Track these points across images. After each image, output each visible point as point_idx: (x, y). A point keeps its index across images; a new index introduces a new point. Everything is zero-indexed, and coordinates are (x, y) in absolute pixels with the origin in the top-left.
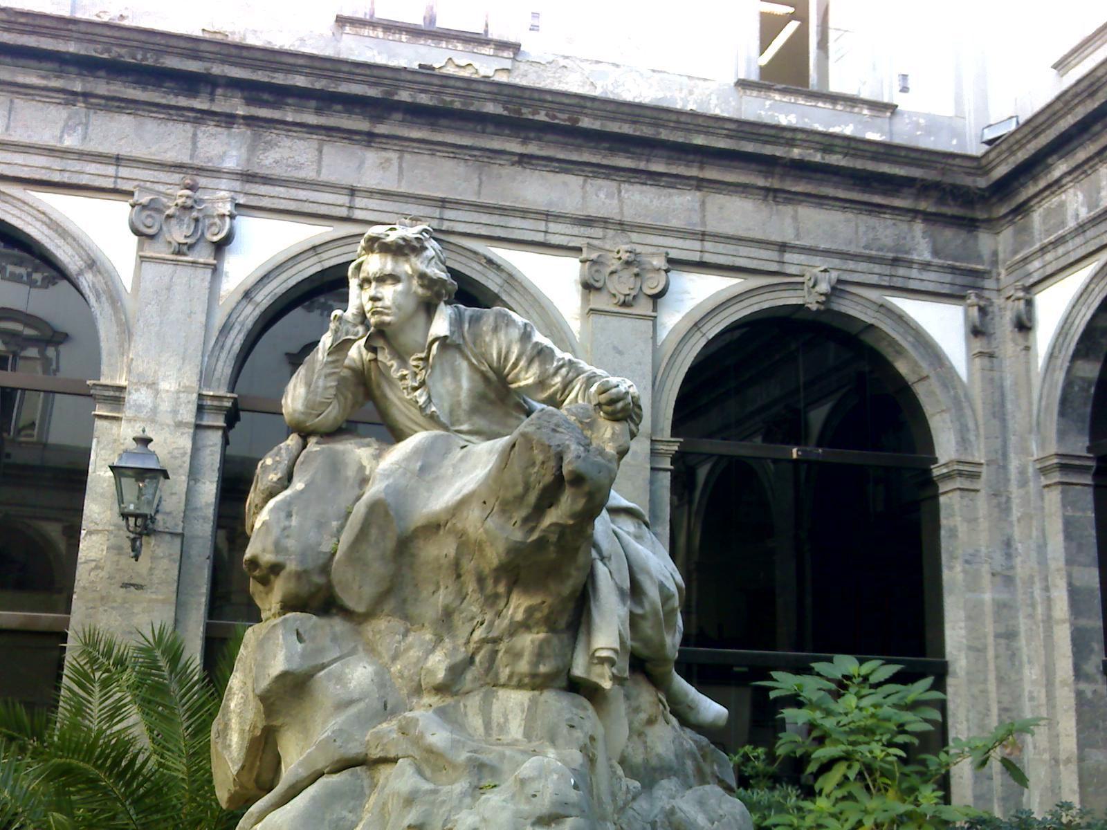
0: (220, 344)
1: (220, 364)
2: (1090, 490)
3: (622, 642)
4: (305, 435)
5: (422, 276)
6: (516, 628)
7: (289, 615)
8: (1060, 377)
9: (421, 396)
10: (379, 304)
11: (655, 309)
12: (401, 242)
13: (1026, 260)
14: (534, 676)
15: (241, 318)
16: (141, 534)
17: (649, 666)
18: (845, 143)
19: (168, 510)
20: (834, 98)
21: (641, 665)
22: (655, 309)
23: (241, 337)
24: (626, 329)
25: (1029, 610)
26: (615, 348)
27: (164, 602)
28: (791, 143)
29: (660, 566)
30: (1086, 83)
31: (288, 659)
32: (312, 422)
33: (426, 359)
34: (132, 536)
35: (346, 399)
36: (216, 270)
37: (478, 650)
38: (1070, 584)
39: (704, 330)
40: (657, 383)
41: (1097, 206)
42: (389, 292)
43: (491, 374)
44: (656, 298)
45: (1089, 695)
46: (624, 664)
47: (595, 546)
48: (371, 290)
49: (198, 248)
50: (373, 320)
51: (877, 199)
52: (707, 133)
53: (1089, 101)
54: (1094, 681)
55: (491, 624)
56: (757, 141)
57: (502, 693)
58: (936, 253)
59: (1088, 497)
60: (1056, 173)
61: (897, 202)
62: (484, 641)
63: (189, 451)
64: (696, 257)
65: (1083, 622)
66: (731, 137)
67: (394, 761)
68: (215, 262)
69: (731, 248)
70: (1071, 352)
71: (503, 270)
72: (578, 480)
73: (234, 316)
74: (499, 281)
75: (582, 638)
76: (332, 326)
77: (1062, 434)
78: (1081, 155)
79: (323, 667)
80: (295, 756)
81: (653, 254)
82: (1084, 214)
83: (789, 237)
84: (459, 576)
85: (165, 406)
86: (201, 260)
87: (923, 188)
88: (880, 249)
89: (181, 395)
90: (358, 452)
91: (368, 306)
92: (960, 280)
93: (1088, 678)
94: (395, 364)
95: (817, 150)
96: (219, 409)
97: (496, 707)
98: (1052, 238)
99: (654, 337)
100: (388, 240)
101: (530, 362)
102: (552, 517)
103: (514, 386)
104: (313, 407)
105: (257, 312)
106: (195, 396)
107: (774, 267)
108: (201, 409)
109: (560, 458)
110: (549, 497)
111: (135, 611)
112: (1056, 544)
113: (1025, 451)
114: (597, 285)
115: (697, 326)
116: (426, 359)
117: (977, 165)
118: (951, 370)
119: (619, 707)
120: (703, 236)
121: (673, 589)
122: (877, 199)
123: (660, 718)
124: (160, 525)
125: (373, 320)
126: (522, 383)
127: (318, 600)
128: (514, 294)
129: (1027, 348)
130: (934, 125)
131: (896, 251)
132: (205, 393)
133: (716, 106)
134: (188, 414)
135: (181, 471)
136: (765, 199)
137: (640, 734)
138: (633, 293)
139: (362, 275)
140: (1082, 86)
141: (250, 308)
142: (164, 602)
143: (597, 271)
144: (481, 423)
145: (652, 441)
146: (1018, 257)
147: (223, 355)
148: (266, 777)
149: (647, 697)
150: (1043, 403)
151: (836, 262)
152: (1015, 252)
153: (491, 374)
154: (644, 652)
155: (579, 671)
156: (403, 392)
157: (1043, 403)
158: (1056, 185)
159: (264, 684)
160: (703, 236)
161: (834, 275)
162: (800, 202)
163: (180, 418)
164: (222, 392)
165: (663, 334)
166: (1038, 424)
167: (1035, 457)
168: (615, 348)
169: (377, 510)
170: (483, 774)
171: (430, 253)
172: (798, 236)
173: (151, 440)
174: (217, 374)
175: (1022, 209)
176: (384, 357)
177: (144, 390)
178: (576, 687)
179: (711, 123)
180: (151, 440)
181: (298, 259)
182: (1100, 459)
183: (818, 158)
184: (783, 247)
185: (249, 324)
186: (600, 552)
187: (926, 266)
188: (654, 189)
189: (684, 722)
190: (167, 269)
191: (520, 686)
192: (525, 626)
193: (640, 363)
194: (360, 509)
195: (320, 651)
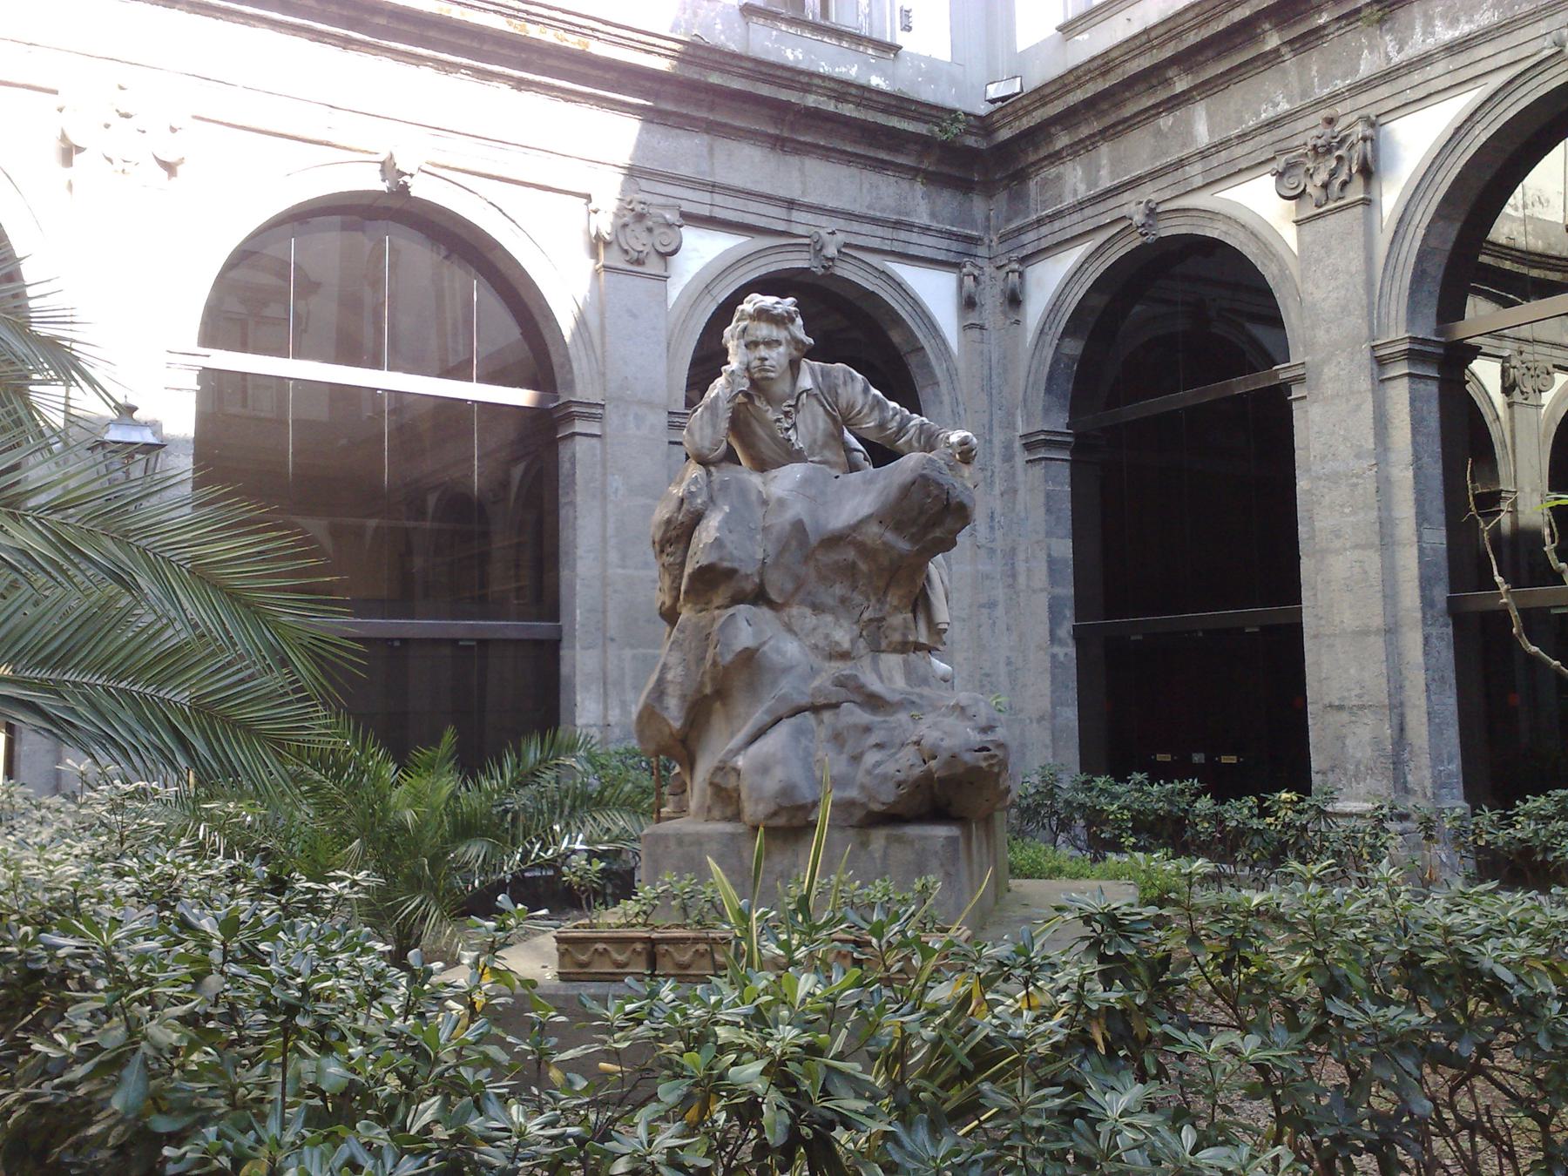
2: (1067, 465)
8: (1049, 353)
13: (1020, 231)
18: (859, 93)
20: (839, 34)
25: (1010, 581)
28: (806, 89)
30: (1100, 62)
38: (1049, 555)
39: (714, 292)
41: (1096, 185)
45: (1061, 658)
51: (883, 155)
52: (722, 71)
53: (1100, 80)
54: (1066, 645)
56: (771, 83)
57: (883, 656)
58: (933, 215)
59: (1065, 472)
60: (1059, 145)
61: (901, 160)
64: (705, 211)
65: (1059, 591)
66: (747, 77)
69: (739, 203)
70: (1061, 329)
77: (1047, 410)
78: (1084, 131)
81: (665, 206)
82: (1083, 192)
83: (795, 194)
87: (925, 144)
88: (883, 210)
92: (955, 246)
93: (1061, 643)
95: (829, 97)
97: (882, 666)
98: (1049, 211)
101: (872, 409)
107: (781, 226)
112: (1039, 515)
113: (1012, 426)
115: (708, 288)
116: (795, 406)
117: (984, 125)
118: (944, 342)
120: (713, 187)
122: (883, 155)
129: (1017, 322)
130: (933, 69)
131: (899, 213)
133: (722, 32)
136: (773, 148)
140: (1095, 64)
146: (1013, 226)
150: (1031, 379)
151: (842, 223)
152: (1009, 220)
157: (1031, 379)
158: (1056, 157)
160: (713, 187)
161: (840, 237)
162: (807, 153)
166: (1025, 400)
167: (1021, 432)
172: (803, 193)
173: (135, 409)
175: (1021, 176)
179: (728, 60)
180: (135, 409)
182: (1076, 436)
183: (831, 106)
184: (791, 204)
187: (925, 230)
188: (661, 129)
191: (895, 651)
193: (654, 329)
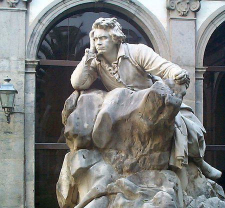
0: (31, 41)
1: (32, 48)
3: (185, 154)
4: (79, 91)
5: (115, 36)
6: (151, 151)
7: (80, 150)
9: (116, 76)
10: (101, 46)
11: (195, 17)
12: (107, 25)
14: (157, 166)
15: (38, 30)
16: (10, 114)
17: (195, 160)
19: (18, 104)
21: (193, 160)
22: (195, 17)
23: (39, 38)
24: (185, 26)
26: (180, 33)
27: (20, 138)
29: (197, 126)
31: (81, 163)
32: (81, 87)
33: (117, 64)
34: (7, 115)
35: (91, 78)
36: (27, 12)
37: (139, 159)
40: (197, 45)
42: (105, 42)
43: (139, 67)
44: (196, 12)
46: (186, 161)
47: (176, 123)
48: (98, 41)
49: (19, 4)
50: (99, 52)
55: (143, 150)
62: (142, 156)
63: (24, 82)
67: (116, 193)
68: (25, 9)
71: (136, 5)
72: (170, 104)
73: (35, 30)
74: (135, 9)
75: (172, 153)
76: (86, 54)
79: (92, 166)
80: (84, 194)
84: (132, 136)
85: (13, 66)
86: (21, 9)
89: (19, 61)
90: (96, 95)
91: (97, 47)
94: (107, 65)
96: (33, 65)
99: (195, 28)
100: (103, 24)
102: (162, 117)
103: (147, 71)
104: (82, 81)
105: (44, 28)
106: (24, 61)
108: (26, 66)
109: (164, 98)
110: (160, 111)
111: (10, 141)
114: (173, 8)
119: (185, 173)
121: (202, 135)
123: (199, 176)
124: (16, 110)
125: (99, 52)
126: (150, 70)
127: (88, 144)
128: (141, 14)
132: (27, 60)
134: (22, 68)
135: (21, 90)
137: (193, 182)
138: (187, 11)
139: (94, 36)
141: (41, 26)
142: (20, 138)
143: (173, 3)
144: (136, 83)
145: (196, 68)
147: (33, 45)
148: (75, 199)
149: (194, 170)
153: (139, 67)
154: (192, 156)
155: (171, 164)
156: (110, 73)
159: (73, 172)
163: (19, 70)
164: (34, 59)
165: (199, 26)
168: (180, 33)
169: (105, 116)
170: (146, 196)
171: (116, 27)
174: (31, 52)
176: (104, 64)
177: (5, 60)
178: (171, 168)
181: (58, 6)
185: (41, 33)
186: (177, 125)
189: (207, 177)
190: (8, 13)
192: (155, 150)
194: (100, 116)
195: (91, 161)
